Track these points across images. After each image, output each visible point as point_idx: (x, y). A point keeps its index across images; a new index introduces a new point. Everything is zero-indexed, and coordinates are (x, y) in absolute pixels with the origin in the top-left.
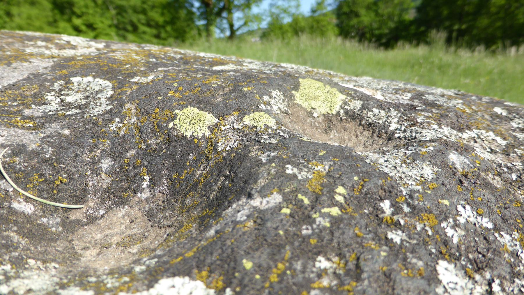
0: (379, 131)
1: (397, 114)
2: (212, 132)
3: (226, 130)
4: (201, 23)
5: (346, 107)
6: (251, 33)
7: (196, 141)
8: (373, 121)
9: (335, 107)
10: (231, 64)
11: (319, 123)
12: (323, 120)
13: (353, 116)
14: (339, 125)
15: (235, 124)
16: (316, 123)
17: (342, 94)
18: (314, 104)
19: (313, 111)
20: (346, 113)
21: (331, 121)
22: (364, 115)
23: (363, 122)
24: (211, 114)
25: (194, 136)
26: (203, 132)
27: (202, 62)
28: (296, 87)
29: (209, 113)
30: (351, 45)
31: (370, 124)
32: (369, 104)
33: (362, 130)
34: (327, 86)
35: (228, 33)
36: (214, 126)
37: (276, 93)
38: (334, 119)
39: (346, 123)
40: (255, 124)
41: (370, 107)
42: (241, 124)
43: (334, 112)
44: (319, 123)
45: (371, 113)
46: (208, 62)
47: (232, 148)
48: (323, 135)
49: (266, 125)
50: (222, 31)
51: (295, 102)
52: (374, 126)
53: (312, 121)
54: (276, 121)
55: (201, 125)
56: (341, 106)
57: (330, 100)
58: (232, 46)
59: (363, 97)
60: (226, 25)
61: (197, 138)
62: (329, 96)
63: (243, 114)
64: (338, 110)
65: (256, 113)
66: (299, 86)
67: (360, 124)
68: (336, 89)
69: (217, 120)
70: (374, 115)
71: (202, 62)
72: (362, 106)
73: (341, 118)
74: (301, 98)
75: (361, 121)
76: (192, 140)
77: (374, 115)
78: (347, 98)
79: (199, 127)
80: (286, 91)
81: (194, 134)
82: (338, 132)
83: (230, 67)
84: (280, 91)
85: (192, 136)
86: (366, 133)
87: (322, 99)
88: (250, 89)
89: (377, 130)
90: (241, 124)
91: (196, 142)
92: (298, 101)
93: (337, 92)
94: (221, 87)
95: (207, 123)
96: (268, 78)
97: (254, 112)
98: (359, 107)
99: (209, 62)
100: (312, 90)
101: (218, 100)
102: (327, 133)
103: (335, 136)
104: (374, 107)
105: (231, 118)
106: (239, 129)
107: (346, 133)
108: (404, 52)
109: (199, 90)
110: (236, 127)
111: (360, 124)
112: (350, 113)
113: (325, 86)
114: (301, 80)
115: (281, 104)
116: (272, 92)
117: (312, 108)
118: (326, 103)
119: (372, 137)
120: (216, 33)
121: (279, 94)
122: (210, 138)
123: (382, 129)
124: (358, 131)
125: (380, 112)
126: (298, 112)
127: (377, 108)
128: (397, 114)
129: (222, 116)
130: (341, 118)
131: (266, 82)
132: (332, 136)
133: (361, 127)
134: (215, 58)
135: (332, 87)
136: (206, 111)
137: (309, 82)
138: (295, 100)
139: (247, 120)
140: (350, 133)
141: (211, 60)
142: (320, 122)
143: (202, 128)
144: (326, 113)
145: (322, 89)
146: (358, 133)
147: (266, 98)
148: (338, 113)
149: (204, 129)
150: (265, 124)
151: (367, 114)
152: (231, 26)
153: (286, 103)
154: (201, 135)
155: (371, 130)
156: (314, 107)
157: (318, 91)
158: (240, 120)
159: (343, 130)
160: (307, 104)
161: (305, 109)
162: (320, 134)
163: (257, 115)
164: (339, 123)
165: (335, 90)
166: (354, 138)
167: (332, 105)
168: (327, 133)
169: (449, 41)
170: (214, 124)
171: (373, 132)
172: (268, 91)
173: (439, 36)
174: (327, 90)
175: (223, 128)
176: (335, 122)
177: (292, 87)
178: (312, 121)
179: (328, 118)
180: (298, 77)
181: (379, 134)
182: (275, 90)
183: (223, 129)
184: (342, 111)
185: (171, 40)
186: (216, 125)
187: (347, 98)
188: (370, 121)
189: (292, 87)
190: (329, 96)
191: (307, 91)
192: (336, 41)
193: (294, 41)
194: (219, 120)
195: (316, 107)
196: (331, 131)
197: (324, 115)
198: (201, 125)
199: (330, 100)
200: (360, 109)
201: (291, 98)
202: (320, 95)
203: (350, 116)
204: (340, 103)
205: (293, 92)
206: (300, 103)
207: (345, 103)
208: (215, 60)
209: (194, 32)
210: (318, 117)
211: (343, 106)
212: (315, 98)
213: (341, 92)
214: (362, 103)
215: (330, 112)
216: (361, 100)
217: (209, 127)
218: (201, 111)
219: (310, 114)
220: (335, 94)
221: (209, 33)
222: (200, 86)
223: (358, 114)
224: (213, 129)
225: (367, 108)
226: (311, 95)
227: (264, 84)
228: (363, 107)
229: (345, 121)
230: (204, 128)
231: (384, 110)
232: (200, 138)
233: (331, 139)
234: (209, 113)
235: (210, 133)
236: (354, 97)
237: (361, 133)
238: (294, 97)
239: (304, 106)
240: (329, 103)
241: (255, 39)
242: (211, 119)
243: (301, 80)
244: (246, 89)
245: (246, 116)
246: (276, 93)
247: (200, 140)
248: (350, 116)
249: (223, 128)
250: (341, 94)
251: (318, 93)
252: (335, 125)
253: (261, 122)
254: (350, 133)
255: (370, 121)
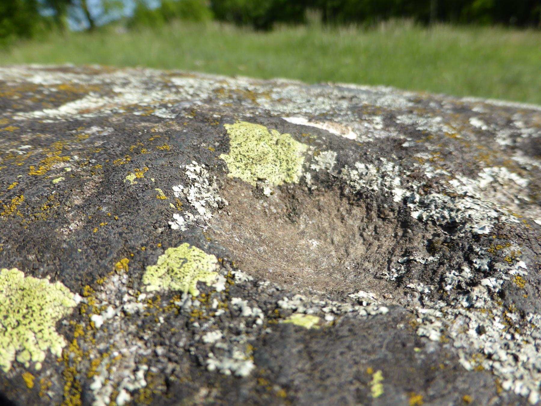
0: (379, 206)
1: (394, 167)
2: (69, 338)
3: (106, 326)
4: (47, 13)
5: (313, 167)
6: (114, 22)
7: (29, 379)
8: (362, 187)
9: (295, 169)
10: (92, 94)
11: (276, 205)
12: (280, 197)
13: (328, 182)
14: (308, 203)
15: (126, 298)
16: (272, 208)
17: (300, 141)
18: (260, 171)
19: (262, 185)
20: (316, 177)
21: (293, 197)
22: (345, 177)
23: (347, 191)
24: (59, 284)
25: (22, 365)
26: (45, 346)
27: (38, 97)
28: (224, 145)
29: (52, 281)
30: (229, 29)
31: (359, 194)
32: (347, 156)
33: (348, 206)
34: (274, 131)
35: (85, 24)
36: (72, 316)
37: (192, 169)
38: (298, 192)
39: (318, 195)
40: (176, 286)
41: (351, 160)
42: (142, 297)
43: (296, 180)
44: (276, 205)
45: (355, 172)
46: (48, 96)
47: (133, 393)
48: (288, 227)
49: (201, 285)
50: (78, 21)
51: (229, 175)
52: (367, 198)
53: (265, 204)
54: (218, 257)
55: (34, 325)
56: (304, 166)
57: (285, 158)
58: (93, 41)
59: (334, 144)
60: (80, 13)
61: (31, 370)
62: (280, 150)
63: (141, 263)
64: (300, 174)
65: (170, 250)
66: (228, 140)
67: (342, 195)
68: (288, 135)
69: (78, 299)
70: (361, 176)
71: (38, 97)
72: (337, 159)
73: (309, 189)
74: (238, 164)
75: (342, 189)
76: (19, 379)
77: (361, 176)
78: (309, 149)
79: (30, 335)
80: (209, 159)
81: (20, 359)
82: (311, 215)
83: (91, 102)
84: (199, 162)
85: (16, 363)
86: (356, 211)
87: (271, 157)
88: (142, 175)
89: (375, 204)
90: (142, 297)
91: (31, 384)
92: (234, 173)
93: (292, 140)
94: (74, 181)
95: (53, 312)
96: (169, 135)
97: (164, 248)
98: (333, 162)
99: (51, 95)
100: (252, 144)
101: (72, 226)
102: (293, 222)
103: (306, 224)
104: (356, 160)
105: (115, 282)
106: (138, 313)
107: (323, 215)
108: (282, 34)
109: (21, 202)
110: (130, 308)
111: (342, 195)
112: (323, 177)
113: (270, 132)
114: (227, 126)
115: (208, 191)
116: (185, 170)
117: (259, 179)
118: (278, 164)
119: (370, 219)
120: (70, 24)
121: (198, 169)
122: (67, 361)
123: (383, 202)
124: (341, 209)
125: (367, 168)
126: (238, 194)
127: (362, 162)
128: (394, 167)
129: (85, 282)
130: (309, 189)
131: (169, 147)
132: (302, 227)
133: (345, 200)
134: (63, 85)
135: (282, 133)
136: (44, 276)
137: (243, 129)
138: (228, 172)
139: (155, 280)
140: (330, 213)
141: (54, 90)
142: (277, 204)
143: (39, 335)
144: (282, 183)
145: (266, 139)
146: (344, 213)
147: (177, 189)
148: (303, 179)
149: (46, 336)
150: (199, 283)
151: (349, 175)
152: (88, 15)
153: (215, 185)
154: (39, 357)
155: (364, 205)
156: (261, 177)
157: (262, 143)
158: (136, 283)
159: (316, 211)
160: (249, 175)
161: (247, 185)
162: (283, 227)
163: (171, 256)
164: (308, 199)
165: (287, 137)
166: (338, 222)
167: (290, 167)
168: (293, 222)
169: (325, 20)
170: (70, 312)
171: (367, 207)
172: (178, 168)
173: (313, 16)
174: (275, 139)
175: (98, 320)
176: (302, 198)
177: (217, 144)
178: (265, 204)
179: (286, 191)
180: (221, 121)
181: (379, 210)
182: (189, 163)
183: (98, 325)
184: (309, 176)
185: (13, 38)
186: (78, 308)
187: (309, 149)
188: (358, 188)
189: (217, 144)
190: (280, 150)
191: (245, 148)
192: (212, 27)
193: (165, 29)
194: (81, 295)
195: (265, 176)
196: (299, 217)
197: (279, 187)
198: (34, 325)
199: (285, 158)
200: (335, 168)
201: (221, 168)
202: (266, 151)
203: (322, 182)
204: (302, 160)
205: (222, 156)
206: (237, 176)
207: (310, 160)
208: (62, 88)
209: (40, 26)
210: (271, 194)
211: (307, 164)
212: (261, 159)
213: (298, 139)
214: (335, 154)
215: (288, 180)
216: (332, 149)
217: (59, 327)
218: (30, 278)
219: (258, 192)
220: (289, 144)
221: (61, 26)
222: (22, 190)
223: (334, 177)
224: (72, 329)
225: (346, 163)
226: (252, 154)
227: (166, 154)
228: (341, 163)
229: (316, 192)
230: (46, 332)
231: (372, 162)
232: (38, 367)
233: (303, 232)
234: (52, 281)
235: (64, 344)
236: (319, 145)
237: (349, 212)
238: (225, 166)
239: (245, 180)
240: (284, 164)
241: (120, 30)
242: (57, 298)
243: (227, 126)
244: (131, 178)
245: (151, 269)
246: (192, 169)
247: (39, 373)
248: (322, 182)
249: (98, 320)
250: (298, 142)
251: (264, 147)
252: (302, 204)
253: (188, 279)
254: (330, 213)
255: (358, 188)
